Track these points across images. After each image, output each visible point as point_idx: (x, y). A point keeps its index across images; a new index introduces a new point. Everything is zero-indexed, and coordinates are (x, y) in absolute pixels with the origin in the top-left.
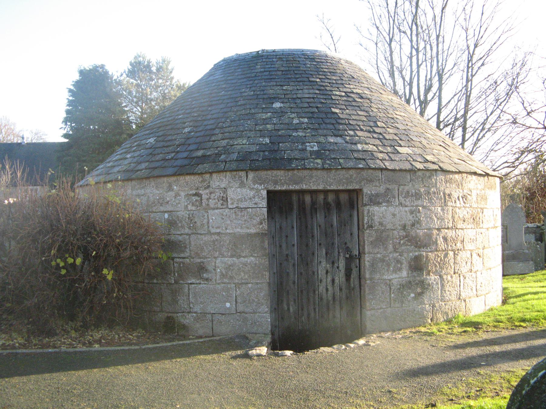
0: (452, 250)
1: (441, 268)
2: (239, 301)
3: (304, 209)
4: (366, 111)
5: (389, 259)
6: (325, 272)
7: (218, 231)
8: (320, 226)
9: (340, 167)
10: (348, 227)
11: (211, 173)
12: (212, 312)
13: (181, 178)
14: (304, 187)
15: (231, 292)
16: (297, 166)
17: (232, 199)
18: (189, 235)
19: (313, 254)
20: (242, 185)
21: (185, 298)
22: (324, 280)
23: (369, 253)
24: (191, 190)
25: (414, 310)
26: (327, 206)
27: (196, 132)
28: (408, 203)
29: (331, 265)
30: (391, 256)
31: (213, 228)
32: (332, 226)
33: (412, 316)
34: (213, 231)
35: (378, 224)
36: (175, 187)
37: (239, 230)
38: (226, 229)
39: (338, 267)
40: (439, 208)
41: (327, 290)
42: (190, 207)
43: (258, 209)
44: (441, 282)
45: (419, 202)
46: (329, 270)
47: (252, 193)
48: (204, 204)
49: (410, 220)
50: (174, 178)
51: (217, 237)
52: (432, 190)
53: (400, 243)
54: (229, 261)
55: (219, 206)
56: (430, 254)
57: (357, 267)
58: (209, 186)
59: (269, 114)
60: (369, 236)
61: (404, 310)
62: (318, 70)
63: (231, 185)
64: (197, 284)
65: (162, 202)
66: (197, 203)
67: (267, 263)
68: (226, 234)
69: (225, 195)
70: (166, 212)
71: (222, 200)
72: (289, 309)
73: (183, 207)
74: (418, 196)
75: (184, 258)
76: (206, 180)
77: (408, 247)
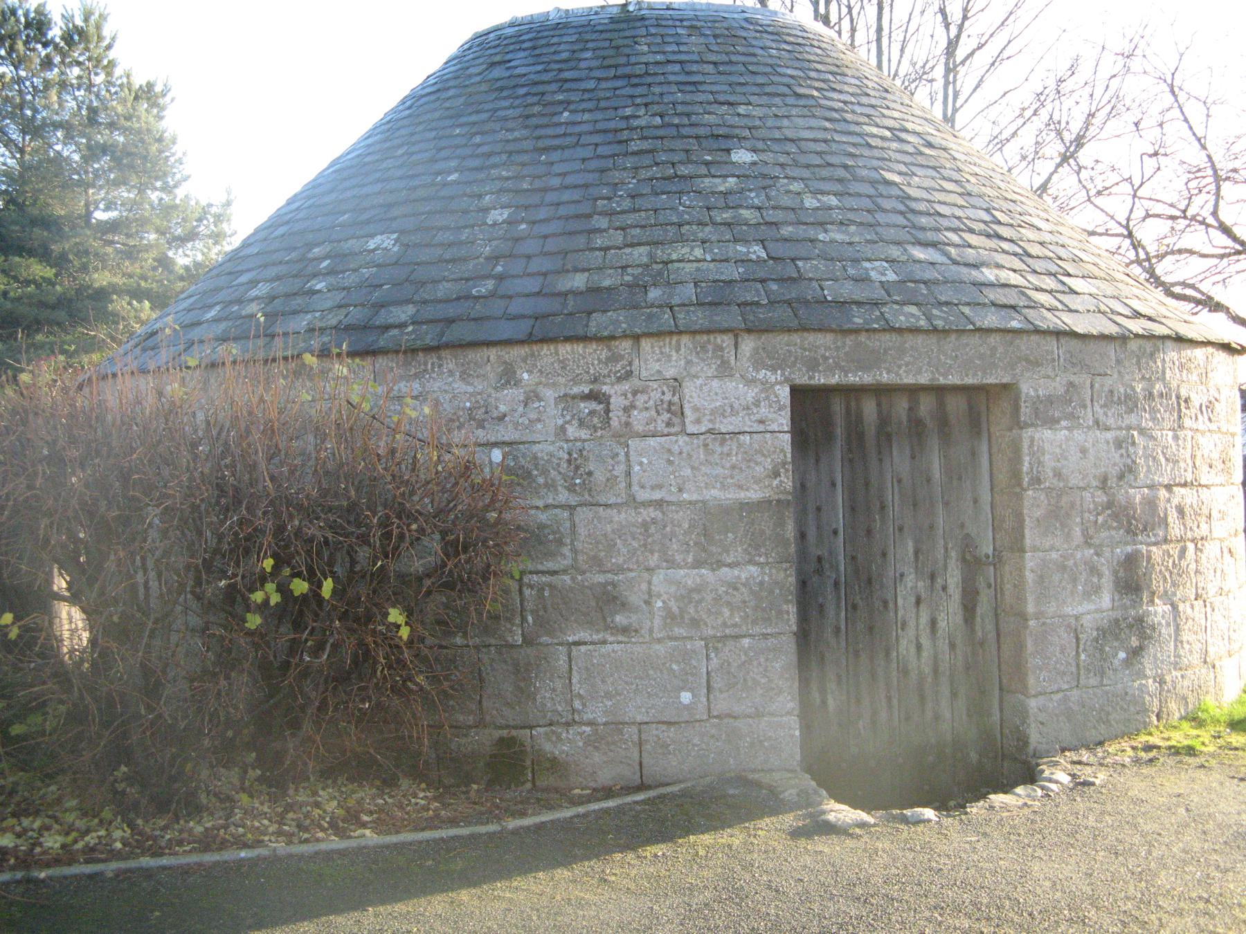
0: (1192, 541)
1: (1174, 584)
2: (718, 683)
3: (861, 436)
4: (956, 182)
5: (1075, 564)
6: (913, 600)
7: (657, 495)
8: (899, 481)
9: (971, 327)
10: (968, 482)
11: (637, 338)
12: (639, 719)
13: (546, 350)
14: (885, 378)
15: (694, 663)
16: (866, 322)
17: (696, 409)
18: (571, 508)
19: (884, 555)
20: (724, 370)
21: (559, 684)
22: (912, 623)
23: (1035, 549)
24: (575, 384)
25: (1126, 694)
26: (917, 428)
27: (534, 223)
28: (1111, 422)
29: (928, 582)
30: (1079, 555)
31: (643, 487)
32: (929, 480)
33: (1122, 708)
34: (643, 495)
35: (1051, 474)
36: (525, 376)
37: (715, 493)
38: (680, 490)
39: (944, 588)
40: (1170, 434)
41: (919, 647)
42: (571, 431)
43: (768, 435)
44: (1175, 620)
45: (1132, 419)
46: (923, 596)
47: (751, 394)
48: (615, 423)
49: (1115, 465)
50: (523, 351)
51: (652, 513)
52: (1157, 386)
53: (1096, 522)
54: (689, 577)
55: (661, 426)
56: (1154, 549)
57: (989, 586)
58: (629, 374)
59: (732, 180)
60: (1034, 504)
61: (1107, 693)
62: (803, 64)
63: (693, 370)
64: (592, 643)
65: (482, 415)
66: (596, 420)
67: (792, 580)
68: (680, 504)
69: (676, 399)
70: (495, 444)
71: (669, 411)
72: (824, 702)
73: (552, 430)
74: (1130, 403)
75: (555, 573)
76: (622, 357)
77: (1113, 533)
